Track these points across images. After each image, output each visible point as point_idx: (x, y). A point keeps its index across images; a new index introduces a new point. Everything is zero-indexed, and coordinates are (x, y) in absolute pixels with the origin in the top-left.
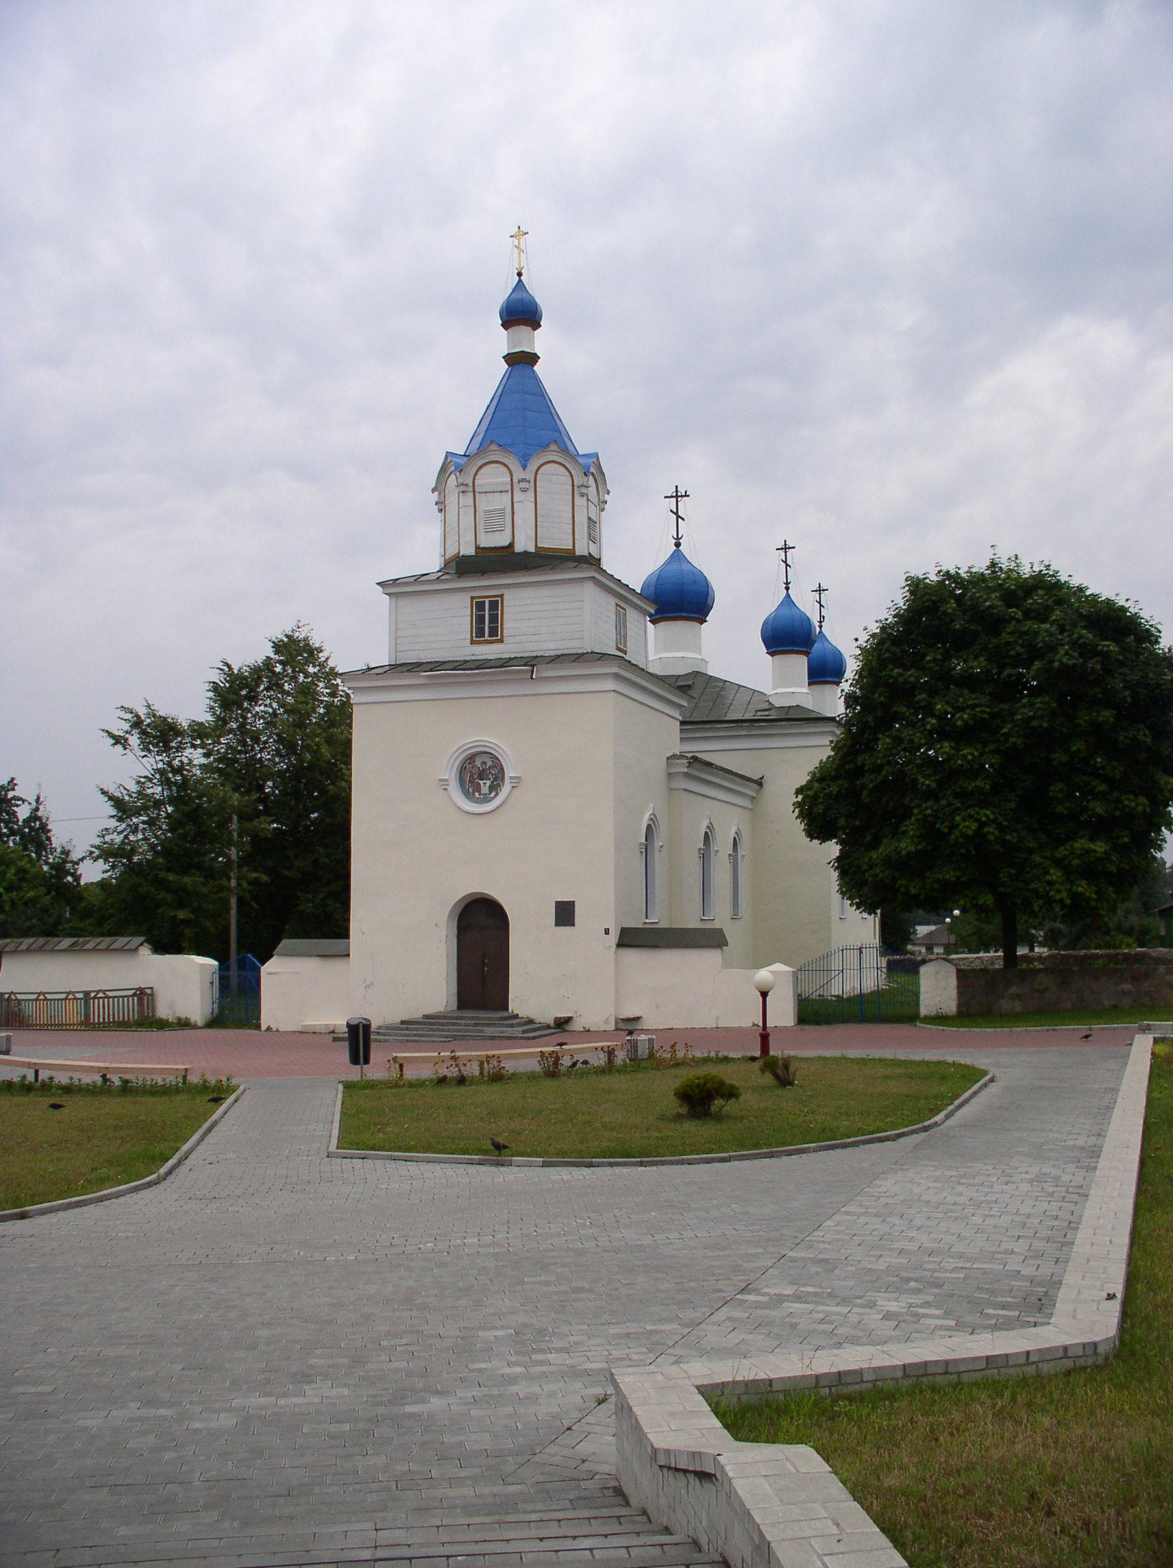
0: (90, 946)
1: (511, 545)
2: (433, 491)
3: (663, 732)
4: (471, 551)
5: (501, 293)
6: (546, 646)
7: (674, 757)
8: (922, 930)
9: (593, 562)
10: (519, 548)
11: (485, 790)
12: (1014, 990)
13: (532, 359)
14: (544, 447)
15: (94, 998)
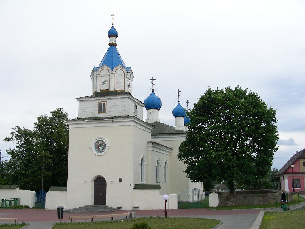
0: (5, 187)
1: (109, 89)
2: (91, 76)
3: (146, 135)
4: (99, 91)
5: (109, 29)
6: (116, 114)
7: (149, 142)
8: (216, 185)
9: (129, 94)
10: (110, 90)
11: (101, 149)
12: (233, 200)
13: (116, 44)
14: (118, 66)
15: (5, 201)
